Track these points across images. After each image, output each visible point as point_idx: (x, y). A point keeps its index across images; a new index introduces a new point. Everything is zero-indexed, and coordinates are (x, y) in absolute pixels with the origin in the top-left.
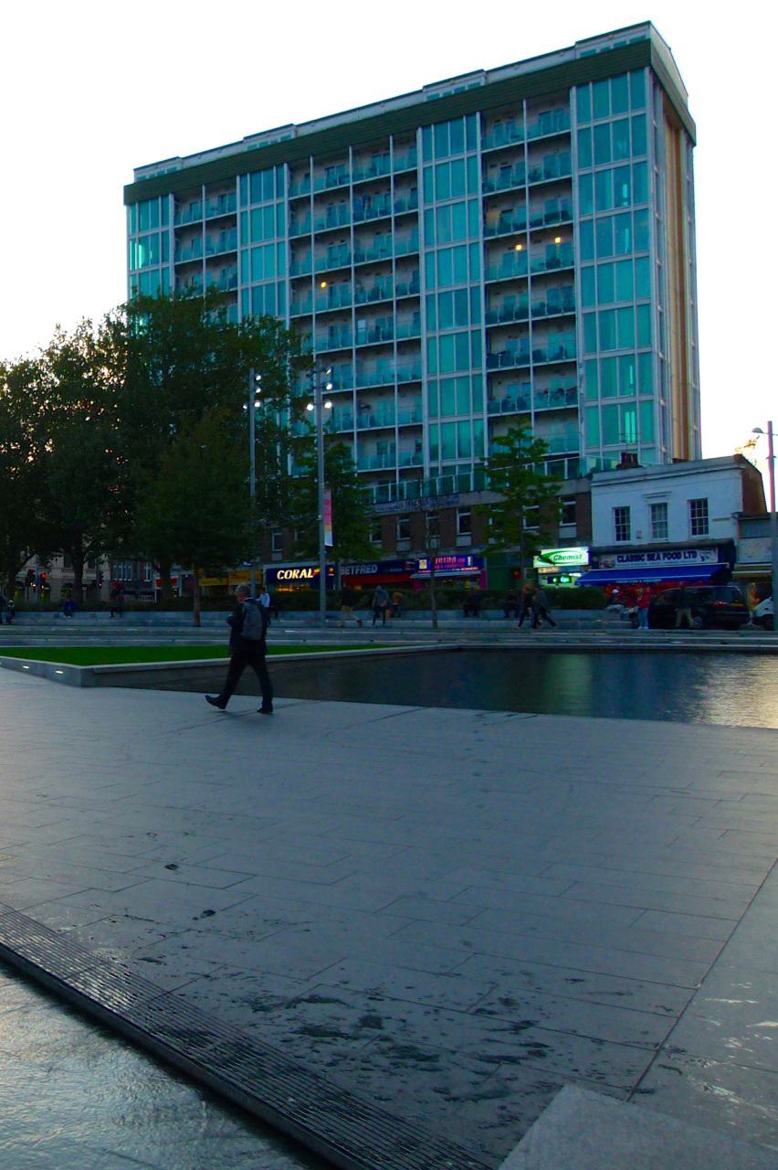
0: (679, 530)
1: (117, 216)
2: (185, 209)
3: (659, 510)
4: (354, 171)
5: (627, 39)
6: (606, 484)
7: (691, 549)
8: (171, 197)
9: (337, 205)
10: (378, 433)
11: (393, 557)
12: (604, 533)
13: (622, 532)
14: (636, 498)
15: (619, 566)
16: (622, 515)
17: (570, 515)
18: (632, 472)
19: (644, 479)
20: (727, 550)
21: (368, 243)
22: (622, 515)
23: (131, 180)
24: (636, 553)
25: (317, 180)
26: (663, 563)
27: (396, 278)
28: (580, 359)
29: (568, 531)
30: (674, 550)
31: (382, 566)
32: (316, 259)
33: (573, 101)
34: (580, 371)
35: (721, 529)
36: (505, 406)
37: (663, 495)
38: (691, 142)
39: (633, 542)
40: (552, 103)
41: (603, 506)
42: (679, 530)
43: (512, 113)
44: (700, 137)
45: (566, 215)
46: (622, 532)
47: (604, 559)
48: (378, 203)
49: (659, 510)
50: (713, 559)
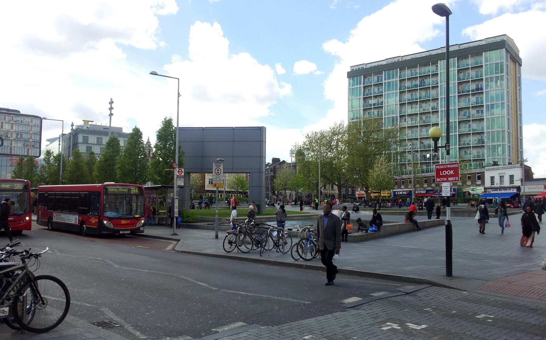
0: (507, 183)
1: (345, 81)
2: (366, 80)
3: (501, 177)
4: (418, 71)
5: (499, 39)
6: (489, 170)
7: (510, 188)
8: (362, 76)
9: (414, 93)
10: (426, 126)
11: (430, 188)
12: (488, 184)
13: (492, 183)
14: (496, 174)
15: (492, 192)
16: (492, 178)
17: (479, 178)
18: (495, 167)
19: (498, 169)
20: (518, 188)
21: (423, 93)
22: (492, 178)
23: (349, 70)
24: (496, 189)
25: (407, 73)
26: (503, 192)
27: (432, 104)
28: (485, 131)
29: (479, 182)
30: (505, 188)
31: (427, 191)
32: (409, 110)
33: (483, 56)
34: (485, 135)
35: (517, 183)
36: (464, 144)
37: (502, 173)
38: (520, 65)
39: (495, 186)
40: (478, 55)
41: (488, 176)
42: (507, 183)
43: (466, 57)
44: (523, 63)
45: (482, 89)
46: (492, 183)
47: (488, 190)
48: (427, 81)
49: (501, 177)
50: (515, 191)
